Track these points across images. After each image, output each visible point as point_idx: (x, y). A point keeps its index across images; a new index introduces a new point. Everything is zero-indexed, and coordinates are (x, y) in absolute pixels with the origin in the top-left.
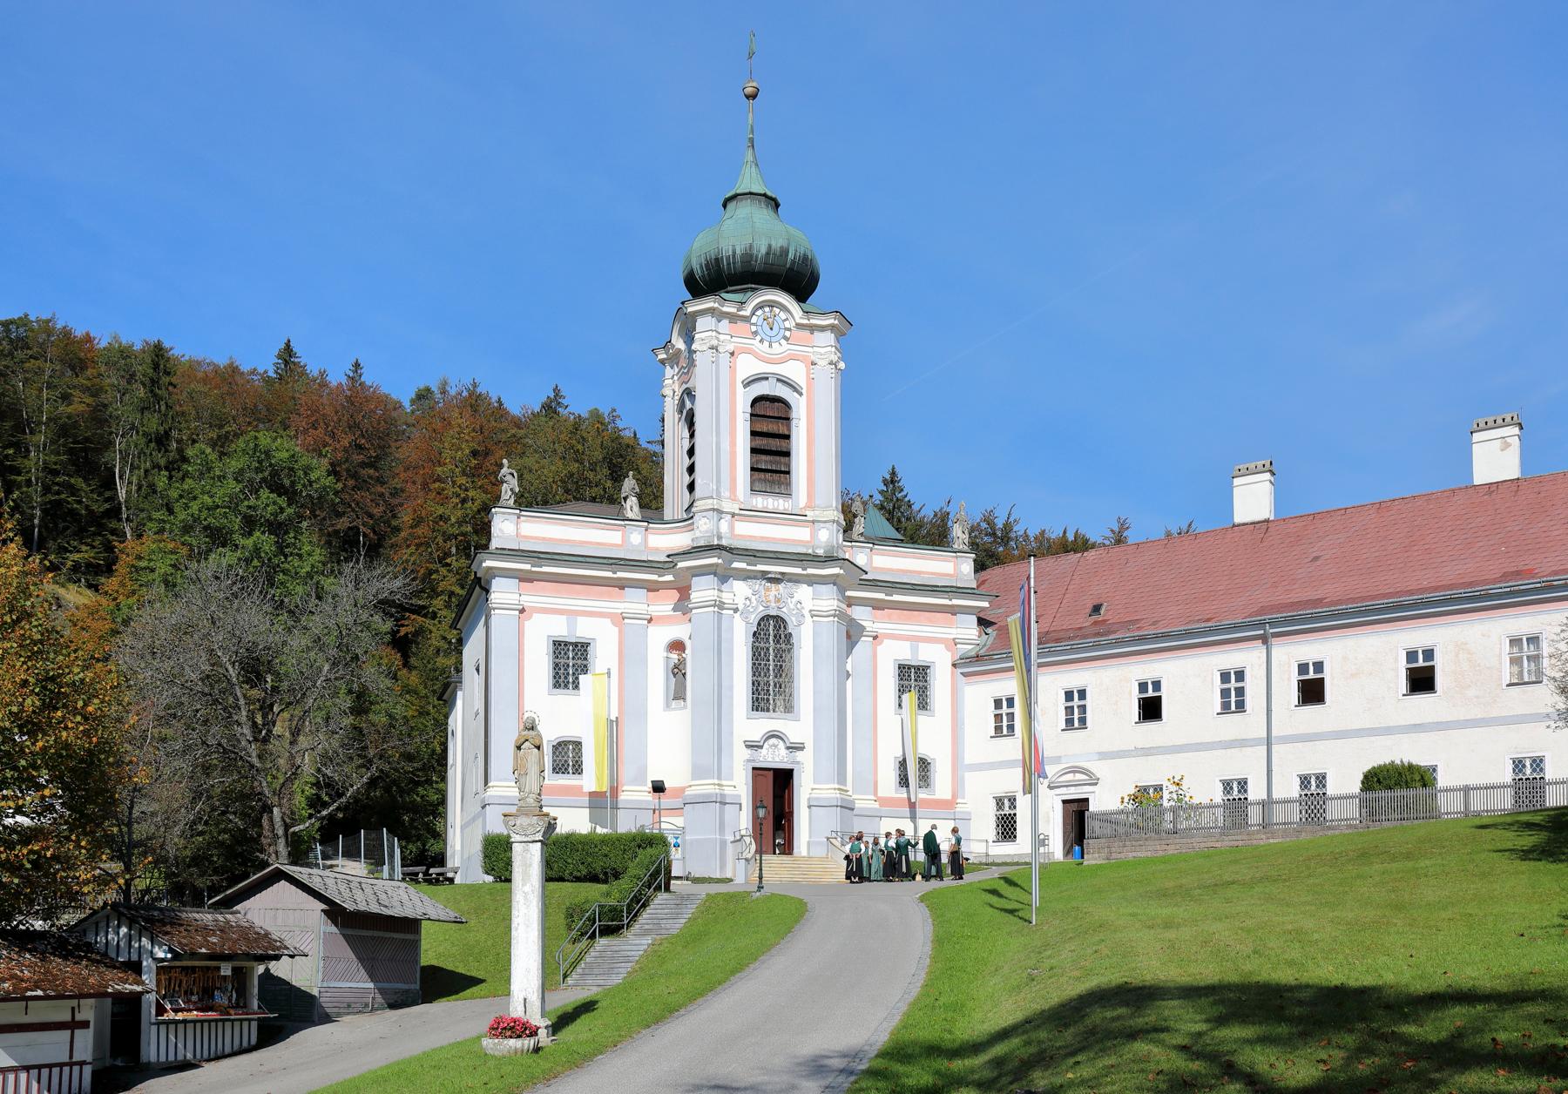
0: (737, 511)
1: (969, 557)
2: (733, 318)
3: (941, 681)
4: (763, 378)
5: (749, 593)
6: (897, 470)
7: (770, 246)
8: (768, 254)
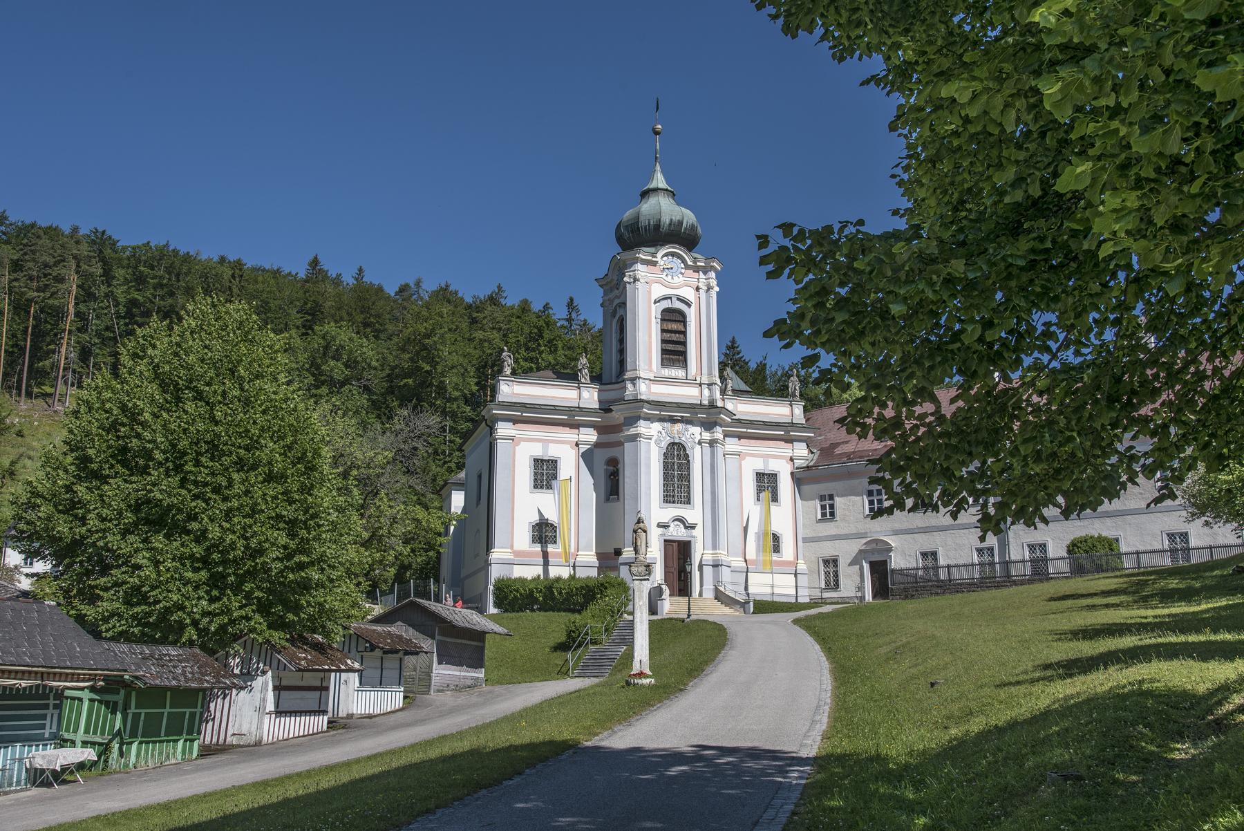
3: (786, 486)
4: (668, 298)
6: (736, 339)
8: (670, 224)
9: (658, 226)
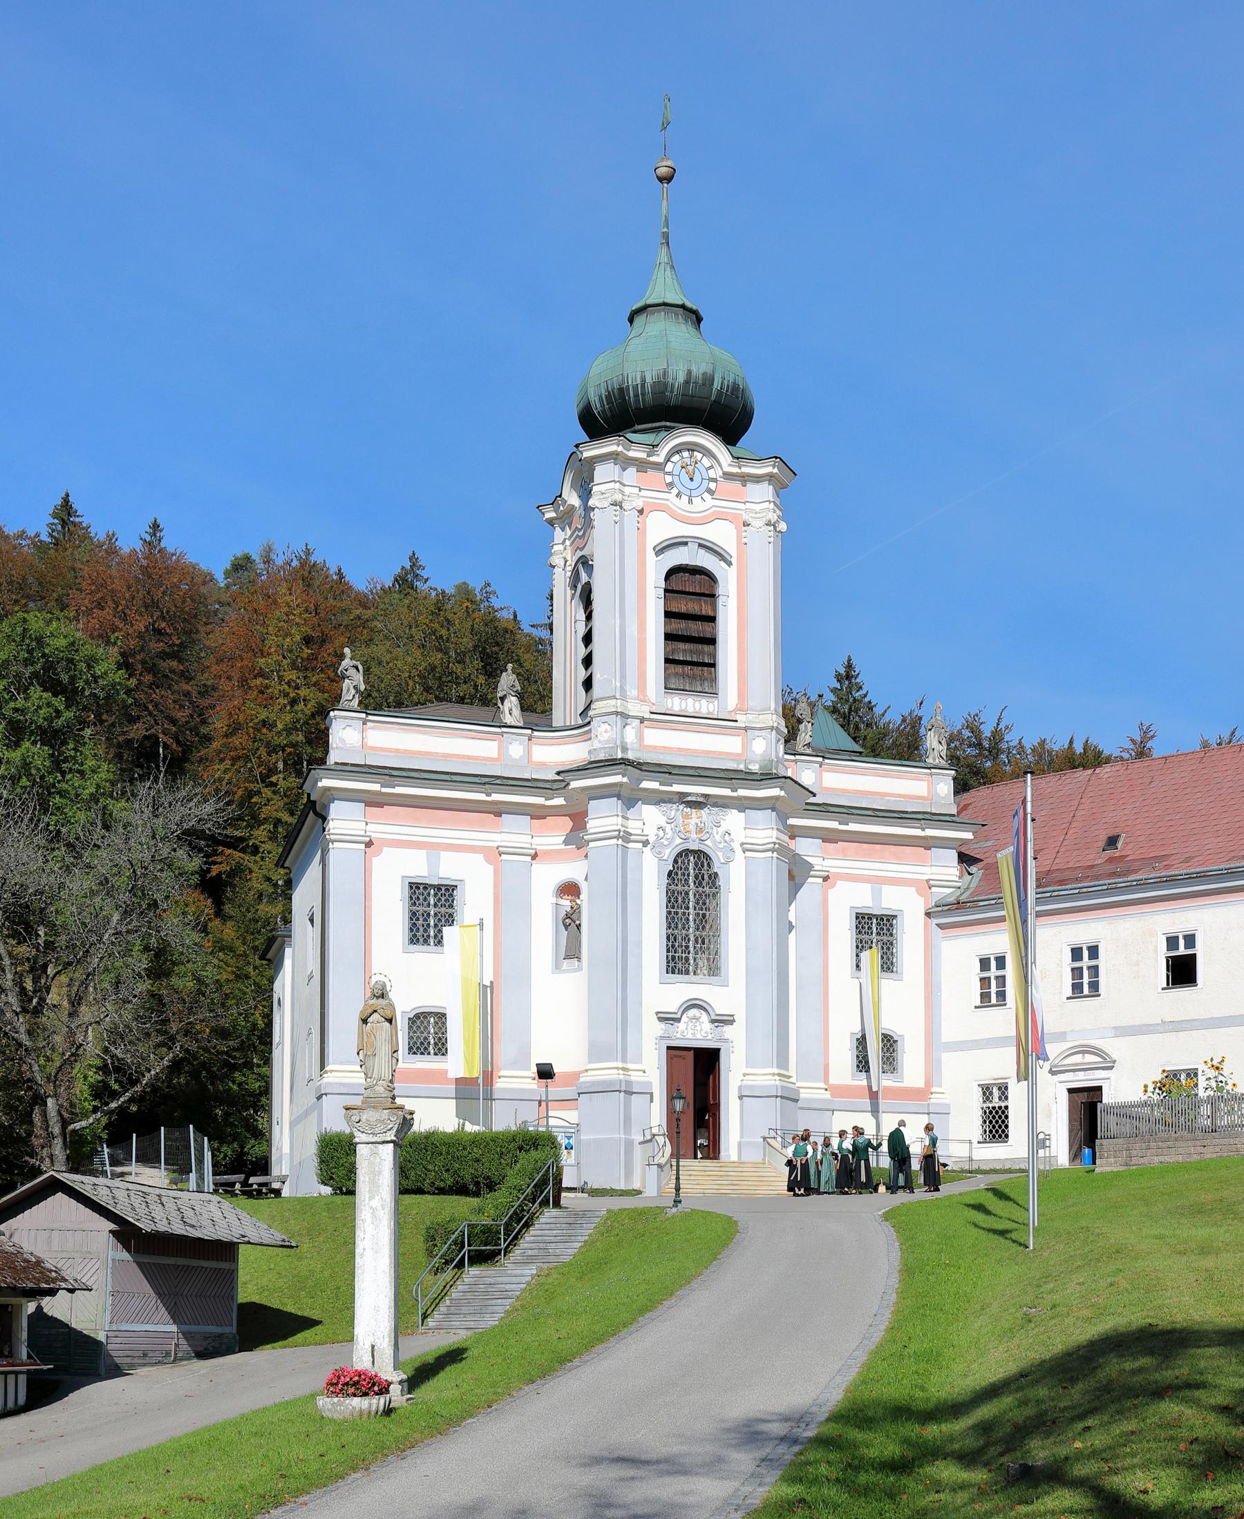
0: (647, 715)
2: (642, 466)
5: (662, 821)
6: (854, 662)
7: (689, 373)
8: (687, 382)
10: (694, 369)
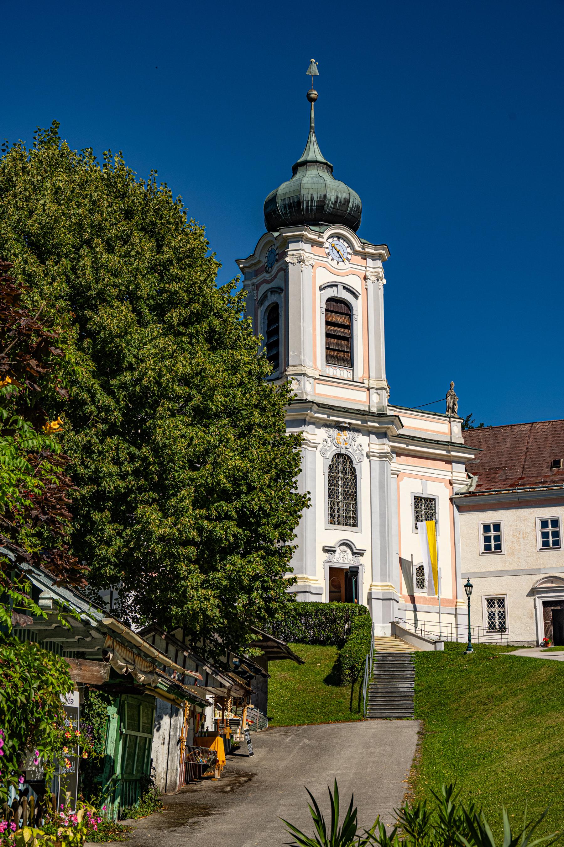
0: (318, 377)
1: (459, 422)
7: (337, 197)
8: (336, 202)
9: (323, 202)
10: (340, 195)
